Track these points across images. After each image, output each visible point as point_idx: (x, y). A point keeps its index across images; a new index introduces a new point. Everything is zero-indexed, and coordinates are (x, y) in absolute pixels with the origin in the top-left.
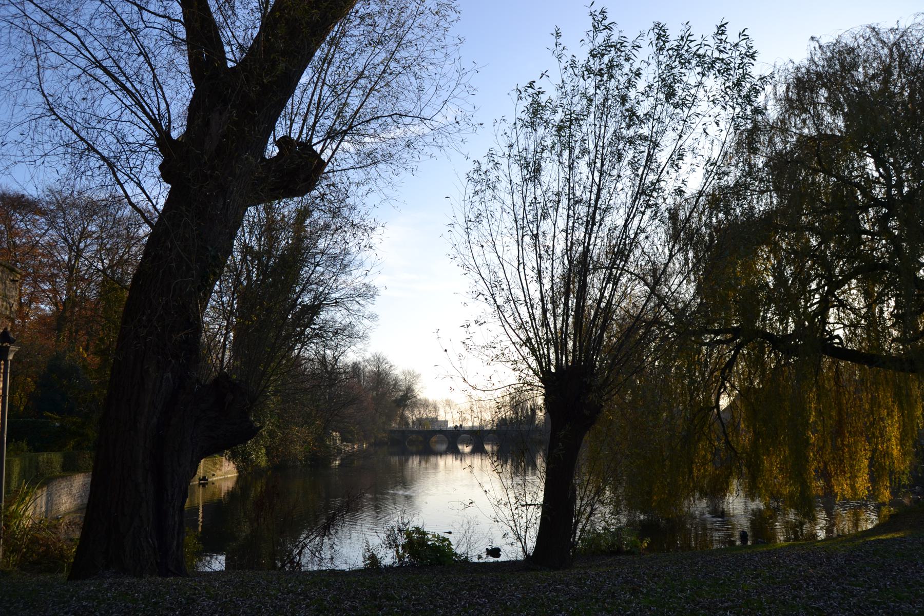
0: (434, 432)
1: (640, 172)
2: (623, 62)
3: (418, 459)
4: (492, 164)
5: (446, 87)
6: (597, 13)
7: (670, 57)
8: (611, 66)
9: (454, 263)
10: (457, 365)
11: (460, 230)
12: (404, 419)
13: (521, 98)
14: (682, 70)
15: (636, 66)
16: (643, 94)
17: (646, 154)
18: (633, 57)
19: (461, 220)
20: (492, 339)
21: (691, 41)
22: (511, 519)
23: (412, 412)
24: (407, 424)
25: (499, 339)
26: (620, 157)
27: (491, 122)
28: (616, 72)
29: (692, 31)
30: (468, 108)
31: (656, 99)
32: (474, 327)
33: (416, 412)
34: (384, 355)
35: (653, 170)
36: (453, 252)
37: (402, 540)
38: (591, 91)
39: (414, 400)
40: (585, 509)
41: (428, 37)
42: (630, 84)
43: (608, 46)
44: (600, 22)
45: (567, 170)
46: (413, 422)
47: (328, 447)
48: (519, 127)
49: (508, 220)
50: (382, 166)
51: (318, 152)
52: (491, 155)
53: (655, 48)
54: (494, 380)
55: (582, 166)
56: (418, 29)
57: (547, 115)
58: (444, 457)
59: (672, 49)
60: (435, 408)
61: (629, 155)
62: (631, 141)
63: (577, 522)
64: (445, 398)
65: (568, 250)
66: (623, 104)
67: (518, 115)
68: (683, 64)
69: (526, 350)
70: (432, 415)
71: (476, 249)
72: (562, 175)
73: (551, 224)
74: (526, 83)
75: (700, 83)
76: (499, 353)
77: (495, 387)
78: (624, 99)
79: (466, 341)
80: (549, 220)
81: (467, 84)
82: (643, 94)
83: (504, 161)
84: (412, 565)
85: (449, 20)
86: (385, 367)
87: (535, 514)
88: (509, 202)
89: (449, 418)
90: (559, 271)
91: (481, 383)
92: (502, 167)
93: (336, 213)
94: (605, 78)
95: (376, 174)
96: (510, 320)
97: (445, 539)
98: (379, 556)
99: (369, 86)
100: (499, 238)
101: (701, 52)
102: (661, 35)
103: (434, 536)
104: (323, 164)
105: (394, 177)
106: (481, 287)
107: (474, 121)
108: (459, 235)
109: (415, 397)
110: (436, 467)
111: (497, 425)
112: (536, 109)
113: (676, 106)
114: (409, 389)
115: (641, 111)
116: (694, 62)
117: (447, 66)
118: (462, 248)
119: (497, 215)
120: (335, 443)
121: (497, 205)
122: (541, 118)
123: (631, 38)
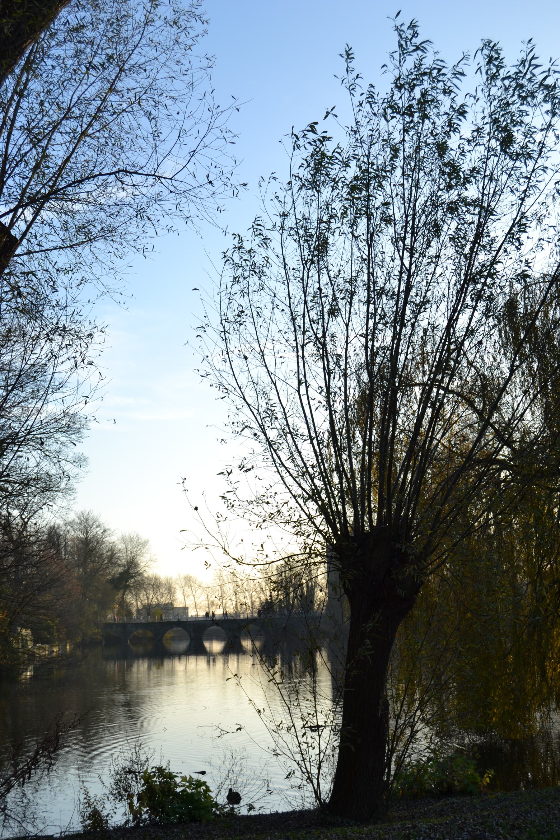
0: (170, 625)
1: (467, 250)
2: (441, 97)
3: (146, 665)
4: (258, 240)
5: (194, 132)
6: (405, 28)
7: (506, 89)
8: (424, 101)
9: (206, 382)
10: (213, 528)
11: (213, 334)
12: (124, 607)
13: (299, 147)
14: (523, 108)
15: (459, 101)
16: (469, 141)
17: (474, 227)
18: (455, 90)
19: (215, 320)
20: (262, 491)
21: (537, 66)
22: (298, 750)
23: (137, 595)
24: (130, 613)
25: (273, 491)
26: (437, 230)
27: (261, 183)
28: (431, 111)
29: (536, 52)
30: (226, 163)
31: (489, 149)
32: (237, 474)
33: (142, 596)
34: (95, 514)
35: (484, 247)
36: (204, 367)
37: (138, 787)
38: (397, 137)
39: (139, 578)
40: (402, 733)
41: (162, 58)
42: (451, 127)
43: (421, 74)
44: (409, 40)
45: (363, 245)
46: (138, 610)
47: (15, 651)
48: (295, 189)
49: (282, 320)
50: (99, 244)
51: (7, 225)
52: (257, 227)
53: (485, 77)
54: (267, 550)
55: (385, 244)
56: (148, 48)
57: (335, 170)
58: (184, 659)
59: (509, 77)
60: (170, 589)
61: (450, 226)
62: (452, 208)
63: (392, 751)
64: (183, 574)
65: (369, 364)
66: (441, 156)
67: (294, 172)
68: (524, 98)
69: (312, 507)
70: (165, 600)
71: (238, 362)
72: (357, 253)
73: (343, 326)
74: (305, 125)
75: (550, 125)
76: (274, 511)
77: (269, 560)
78: (442, 148)
79: (227, 495)
80: (339, 319)
81: (223, 128)
82: (469, 141)
83: (275, 236)
84: (153, 824)
85: (193, 34)
86: (96, 531)
87: (328, 740)
88: (282, 293)
89: (189, 603)
90: (354, 394)
91: (250, 556)
92: (272, 245)
93: (32, 312)
94: (416, 118)
95: (91, 255)
96: (289, 464)
97: (200, 784)
98: (104, 813)
99: (79, 130)
100: (269, 345)
101: (550, 81)
102: (494, 59)
103: (184, 779)
104: (15, 243)
105: (117, 261)
106: (246, 416)
107: (235, 180)
108: (212, 341)
109: (140, 574)
110: (172, 673)
111: (259, 612)
112: (320, 162)
113: (516, 157)
114: (132, 563)
115: (466, 166)
116: (540, 96)
117: (194, 104)
118: (217, 360)
119: (266, 313)
120: (25, 646)
121: (265, 299)
122: (327, 175)
123: (450, 63)
